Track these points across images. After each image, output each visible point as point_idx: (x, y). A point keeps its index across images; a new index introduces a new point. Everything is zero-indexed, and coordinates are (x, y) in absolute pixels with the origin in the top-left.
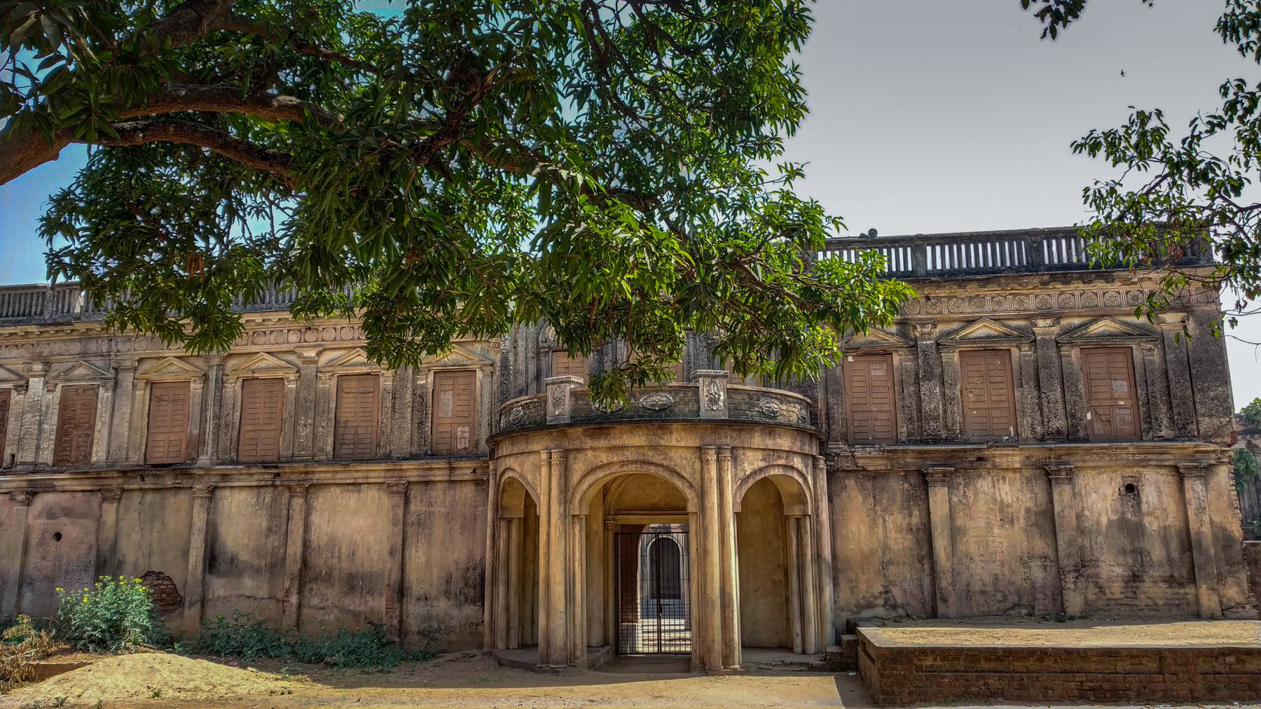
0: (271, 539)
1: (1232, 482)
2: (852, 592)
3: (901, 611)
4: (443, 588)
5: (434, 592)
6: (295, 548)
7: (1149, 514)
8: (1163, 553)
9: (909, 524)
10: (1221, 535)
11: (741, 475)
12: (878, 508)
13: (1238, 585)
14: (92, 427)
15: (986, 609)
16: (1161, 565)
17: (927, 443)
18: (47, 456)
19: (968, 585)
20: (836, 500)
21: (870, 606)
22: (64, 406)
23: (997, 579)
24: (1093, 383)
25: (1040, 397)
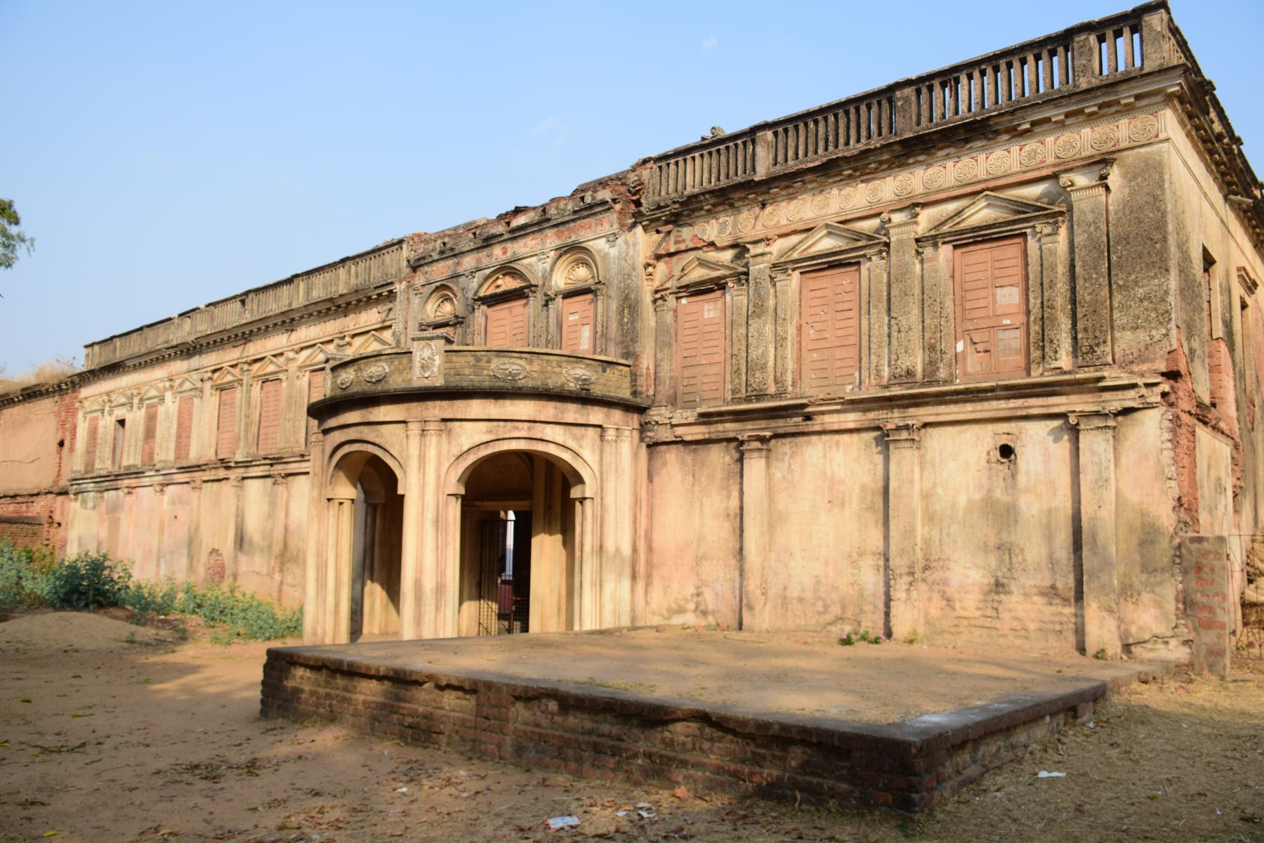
2: (665, 593)
3: (711, 619)
6: (279, 533)
7: (1027, 490)
8: (1044, 551)
9: (727, 508)
10: (1138, 523)
11: (456, 451)
12: (696, 488)
13: (1159, 605)
15: (803, 622)
20: (656, 480)
21: (681, 611)
23: (818, 582)
25: (890, 327)
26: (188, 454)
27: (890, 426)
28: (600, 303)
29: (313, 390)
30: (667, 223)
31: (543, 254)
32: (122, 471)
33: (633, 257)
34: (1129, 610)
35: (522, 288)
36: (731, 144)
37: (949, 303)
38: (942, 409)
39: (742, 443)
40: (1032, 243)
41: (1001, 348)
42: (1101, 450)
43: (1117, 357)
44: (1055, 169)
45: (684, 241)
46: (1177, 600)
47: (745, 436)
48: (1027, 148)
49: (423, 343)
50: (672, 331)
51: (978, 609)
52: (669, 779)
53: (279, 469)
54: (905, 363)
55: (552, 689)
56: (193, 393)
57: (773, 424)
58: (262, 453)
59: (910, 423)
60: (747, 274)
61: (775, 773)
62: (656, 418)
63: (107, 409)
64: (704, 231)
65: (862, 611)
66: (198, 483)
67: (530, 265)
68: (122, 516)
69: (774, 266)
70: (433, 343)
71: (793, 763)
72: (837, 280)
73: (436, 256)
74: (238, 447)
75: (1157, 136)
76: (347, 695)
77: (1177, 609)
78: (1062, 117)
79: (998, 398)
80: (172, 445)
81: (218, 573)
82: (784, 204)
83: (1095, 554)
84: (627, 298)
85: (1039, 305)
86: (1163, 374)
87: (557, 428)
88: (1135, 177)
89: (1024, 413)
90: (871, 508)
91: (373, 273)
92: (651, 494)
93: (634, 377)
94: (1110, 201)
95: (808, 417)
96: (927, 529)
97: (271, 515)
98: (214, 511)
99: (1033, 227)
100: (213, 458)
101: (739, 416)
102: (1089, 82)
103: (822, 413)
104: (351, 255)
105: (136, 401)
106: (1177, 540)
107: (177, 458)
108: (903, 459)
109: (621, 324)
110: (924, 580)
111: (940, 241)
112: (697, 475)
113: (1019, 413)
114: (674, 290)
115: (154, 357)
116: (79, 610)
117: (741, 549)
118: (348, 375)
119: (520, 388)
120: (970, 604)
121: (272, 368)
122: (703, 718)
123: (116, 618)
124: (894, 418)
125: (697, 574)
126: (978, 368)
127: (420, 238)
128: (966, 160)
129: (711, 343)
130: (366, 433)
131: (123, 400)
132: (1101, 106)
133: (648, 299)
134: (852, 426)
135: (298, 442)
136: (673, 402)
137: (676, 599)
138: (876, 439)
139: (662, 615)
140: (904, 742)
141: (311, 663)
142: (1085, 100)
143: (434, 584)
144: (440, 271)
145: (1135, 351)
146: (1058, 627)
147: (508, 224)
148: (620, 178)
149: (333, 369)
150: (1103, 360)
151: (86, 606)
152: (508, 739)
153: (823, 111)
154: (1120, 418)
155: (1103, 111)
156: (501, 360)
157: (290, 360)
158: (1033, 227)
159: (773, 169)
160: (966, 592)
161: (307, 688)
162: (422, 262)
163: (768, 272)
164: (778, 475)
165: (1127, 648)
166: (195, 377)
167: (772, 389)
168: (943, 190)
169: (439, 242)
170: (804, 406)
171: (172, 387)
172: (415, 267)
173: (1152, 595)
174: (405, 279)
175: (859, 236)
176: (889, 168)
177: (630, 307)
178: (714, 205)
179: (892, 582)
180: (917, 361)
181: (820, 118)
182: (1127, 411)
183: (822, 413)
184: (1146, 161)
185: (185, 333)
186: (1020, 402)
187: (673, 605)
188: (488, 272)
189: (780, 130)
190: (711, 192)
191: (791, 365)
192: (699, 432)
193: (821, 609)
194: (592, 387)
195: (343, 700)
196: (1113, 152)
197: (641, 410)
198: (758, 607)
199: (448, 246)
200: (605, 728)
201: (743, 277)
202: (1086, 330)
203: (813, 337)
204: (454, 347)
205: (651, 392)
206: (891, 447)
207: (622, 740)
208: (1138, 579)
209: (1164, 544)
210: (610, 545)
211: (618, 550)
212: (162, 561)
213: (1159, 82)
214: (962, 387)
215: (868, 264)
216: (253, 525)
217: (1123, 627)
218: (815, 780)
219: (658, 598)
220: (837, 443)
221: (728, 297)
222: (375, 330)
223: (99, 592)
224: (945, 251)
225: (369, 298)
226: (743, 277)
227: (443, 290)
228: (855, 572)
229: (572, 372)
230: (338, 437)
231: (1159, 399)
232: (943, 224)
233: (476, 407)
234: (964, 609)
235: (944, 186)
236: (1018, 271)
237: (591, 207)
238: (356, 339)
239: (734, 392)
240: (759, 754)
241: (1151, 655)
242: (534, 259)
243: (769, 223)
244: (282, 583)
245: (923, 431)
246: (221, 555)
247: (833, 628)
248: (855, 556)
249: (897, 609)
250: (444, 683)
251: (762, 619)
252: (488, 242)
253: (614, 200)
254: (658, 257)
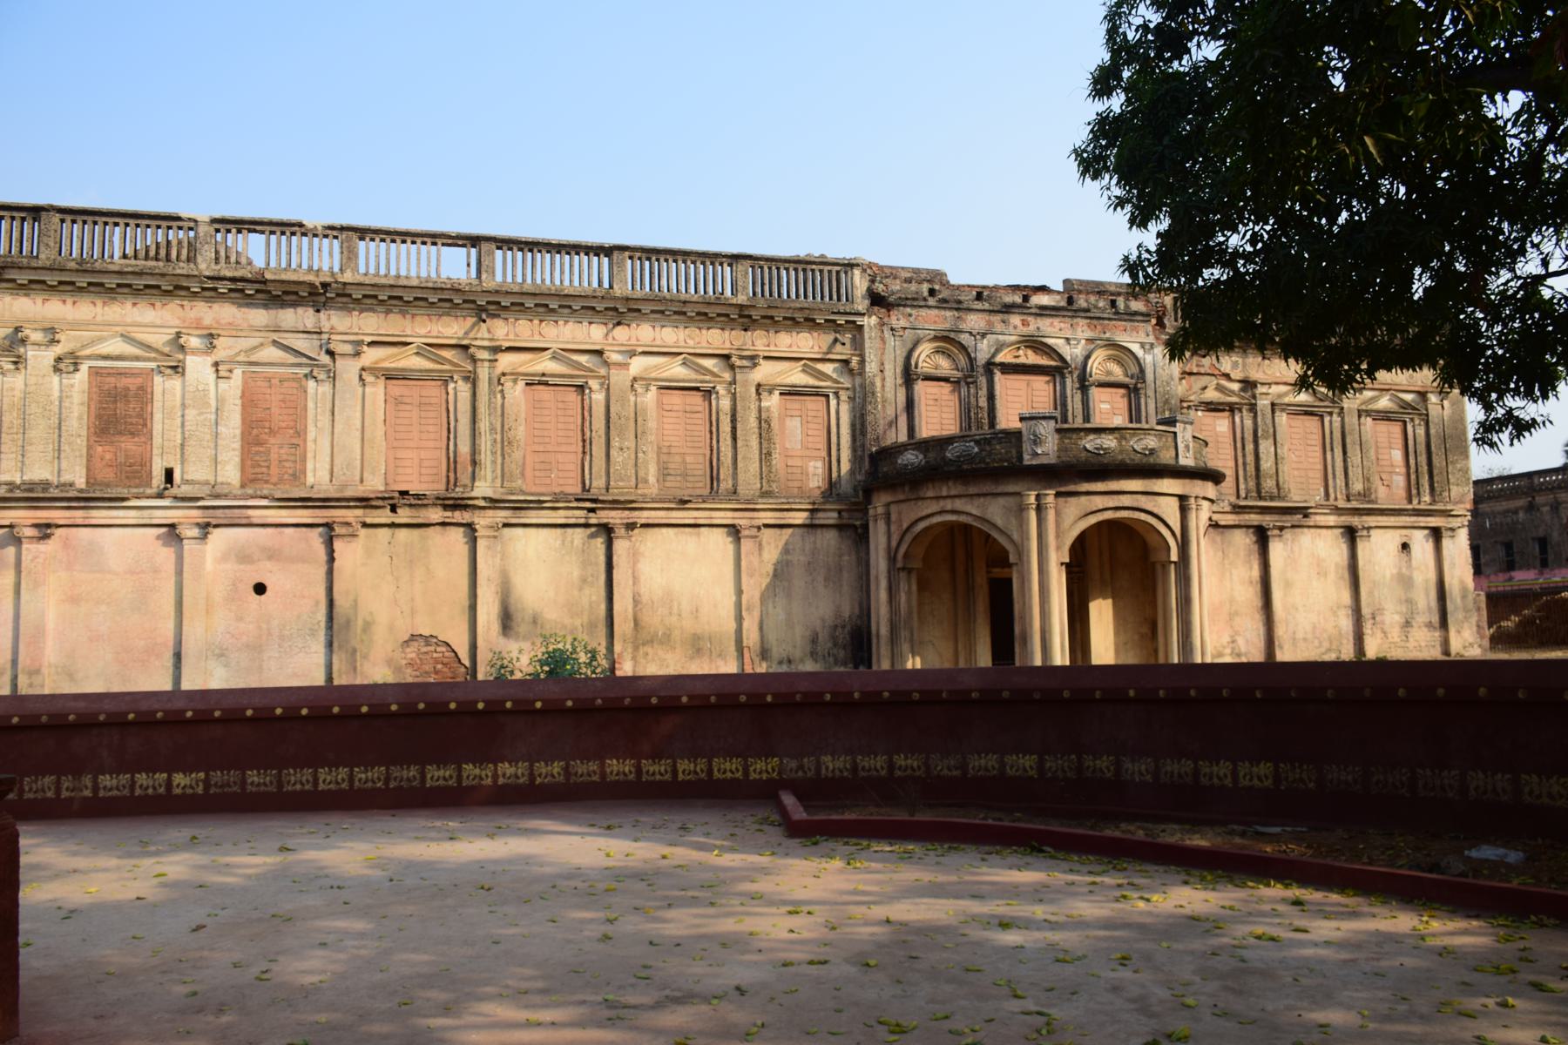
0: (587, 591)
4: (808, 649)
5: (798, 654)
14: (301, 433)
18: (230, 474)
22: (249, 401)
95: (1306, 516)
130: (1144, 502)
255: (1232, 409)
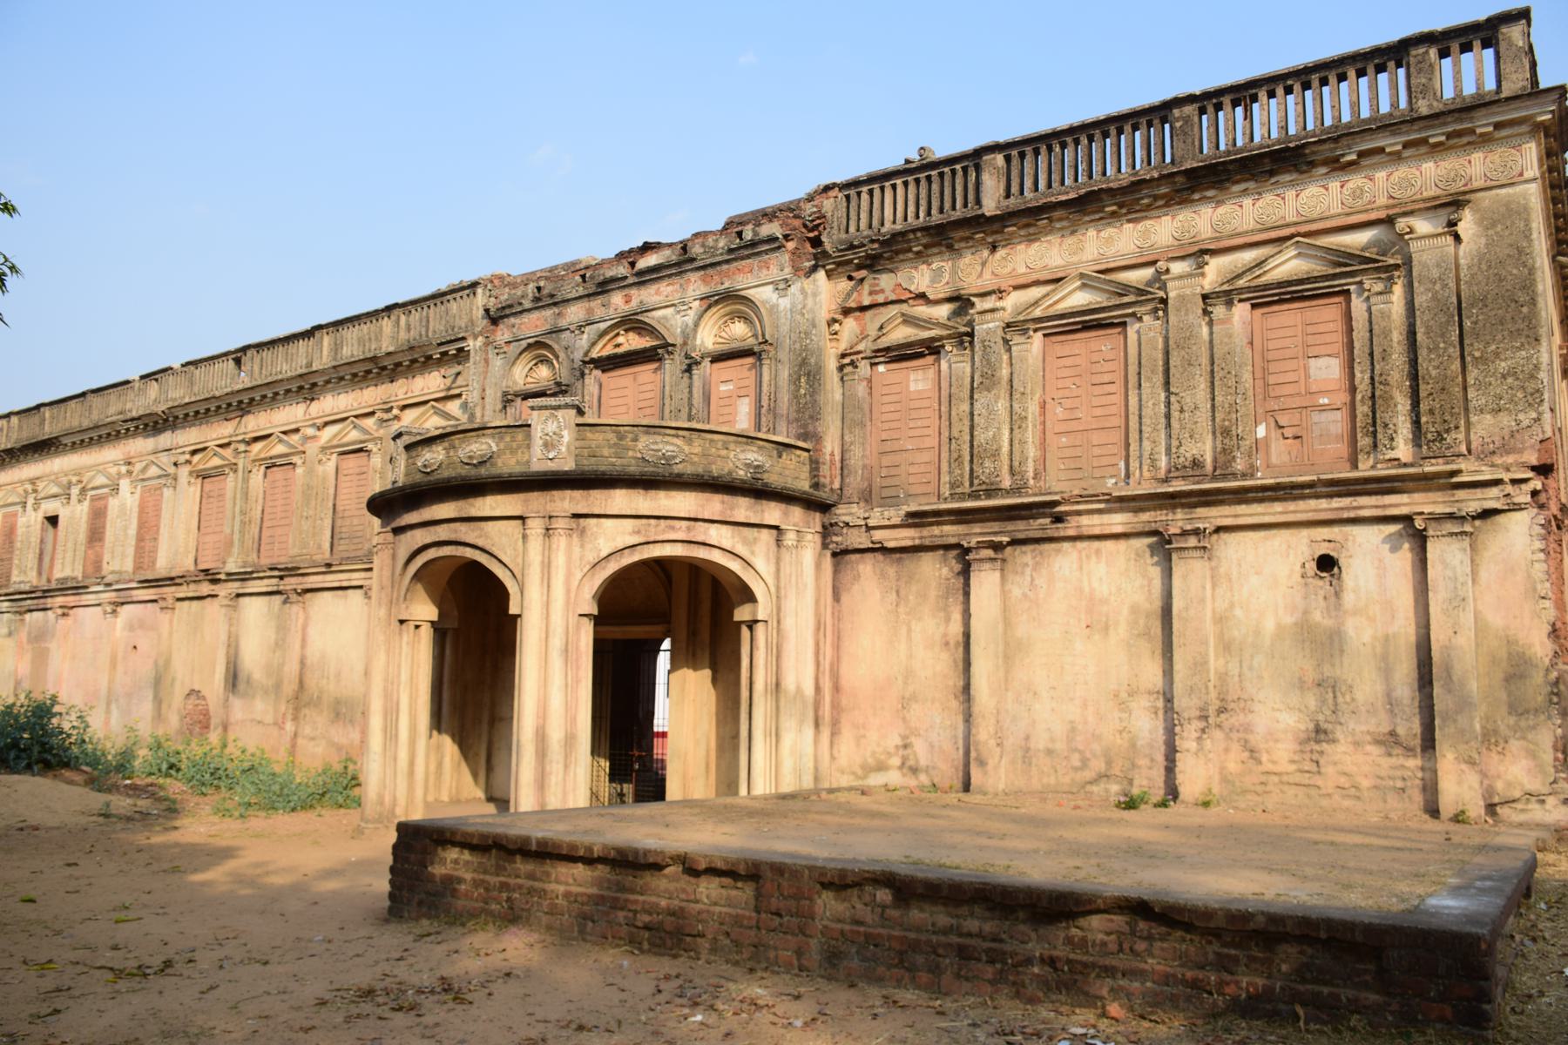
1: (1539, 545)
2: (858, 745)
6: (292, 668)
7: (1356, 612)
8: (1380, 688)
9: (945, 635)
10: (1503, 653)
11: (592, 557)
12: (901, 609)
13: (1532, 755)
15: (1052, 780)
16: (1372, 710)
17: (978, 498)
19: (1027, 738)
20: (845, 598)
21: (881, 767)
23: (1073, 730)
24: (1272, 367)
25: (1168, 404)
26: (154, 563)
27: (1172, 531)
28: (765, 370)
29: (342, 478)
30: (859, 267)
31: (684, 304)
32: (53, 585)
33: (812, 311)
34: (1493, 761)
35: (654, 348)
36: (946, 170)
37: (1247, 376)
38: (1242, 509)
39: (968, 551)
40: (1358, 304)
41: (1316, 433)
42: (1456, 562)
43: (1473, 446)
44: (1391, 212)
45: (882, 291)
46: (1556, 749)
47: (974, 541)
48: (1351, 185)
49: (547, 413)
50: (866, 407)
51: (1293, 762)
52: (1086, 994)
53: (291, 583)
54: (1190, 450)
55: (883, 873)
56: (162, 481)
57: (1010, 526)
58: (265, 561)
59: (1201, 526)
60: (971, 335)
61: (1260, 982)
62: (846, 519)
63: (31, 501)
64: (911, 279)
65: (1134, 765)
66: (170, 601)
67: (665, 318)
68: (53, 645)
69: (1008, 325)
70: (560, 413)
71: (1284, 967)
72: (1094, 345)
73: (527, 304)
74: (229, 554)
75: (1521, 174)
76: (537, 884)
77: (1556, 759)
78: (1399, 147)
79: (1317, 497)
80: (131, 551)
81: (201, 722)
82: (1021, 247)
83: (1450, 691)
84: (804, 362)
85: (1367, 380)
86: (1533, 468)
87: (724, 529)
88: (1493, 225)
89: (1352, 514)
90: (1146, 634)
91: (436, 324)
92: (838, 617)
93: (815, 465)
94: (1461, 253)
95: (1059, 519)
96: (1221, 661)
97: (280, 644)
98: (192, 640)
99: (1361, 283)
100: (192, 568)
101: (963, 516)
102: (1430, 106)
103: (1079, 513)
104: (400, 301)
105: (75, 491)
106: (1554, 674)
107: (138, 567)
108: (1190, 573)
109: (796, 396)
110: (1219, 726)
111: (1236, 298)
112: (903, 593)
113: (1346, 515)
114: (869, 354)
115: (104, 432)
116: (18, 773)
117: (967, 688)
118: (434, 456)
119: (679, 475)
120: (1282, 755)
121: (281, 449)
122: (1139, 909)
123: (71, 782)
124: (1177, 520)
125: (904, 719)
126: (1286, 458)
127: (501, 280)
128: (1269, 198)
129: (919, 423)
130: (464, 532)
131: (55, 490)
132: (1449, 136)
133: (832, 364)
134: (1119, 529)
135: (320, 547)
136: (867, 497)
137: (874, 753)
138: (1150, 546)
139: (853, 773)
140: (1469, 935)
141: (475, 841)
142: (1432, 127)
143: (562, 735)
144: (533, 324)
145: (1496, 439)
146: (1399, 784)
147: (633, 264)
148: (791, 209)
149: (408, 448)
150: (1455, 450)
151: (29, 767)
152: (813, 942)
153: (1073, 131)
154: (1477, 523)
155: (1451, 142)
156: (652, 439)
157: (307, 438)
158: (1361, 283)
159: (1005, 203)
160: (1277, 741)
161: (468, 876)
162: (508, 311)
163: (1000, 332)
164: (1016, 592)
165: (1491, 808)
166: (165, 459)
167: (1007, 483)
168: (1239, 234)
169: (532, 286)
170: (1055, 504)
171: (130, 473)
172: (495, 318)
173: (1522, 742)
174: (481, 333)
175: (1126, 289)
176: (1167, 205)
177: (808, 375)
178: (926, 246)
179: (1178, 729)
180: (1205, 448)
181: (1069, 140)
182: (1487, 514)
183: (1079, 513)
184: (1507, 205)
185: (151, 400)
186: (1346, 502)
187: (870, 760)
188: (603, 326)
189: (1014, 153)
190: (925, 229)
191: (1032, 452)
192: (907, 537)
193: (1078, 764)
194: (765, 476)
195: (531, 891)
196: (1465, 193)
197: (824, 507)
198: (991, 763)
199: (545, 292)
200: (972, 925)
201: (965, 339)
202: (1431, 412)
203: (1061, 417)
204: (588, 419)
205: (836, 485)
206: (1174, 556)
207: (1001, 941)
208: (1505, 722)
209: (1538, 678)
210: (789, 683)
211: (799, 690)
212: (113, 706)
213: (1527, 107)
214: (1272, 481)
215: (1137, 325)
216: (253, 656)
217: (1486, 782)
218: (1326, 990)
219: (848, 753)
220: (1098, 552)
221: (944, 365)
222: (436, 400)
223: (45, 747)
224: (1241, 311)
225: (429, 358)
226: (965, 339)
227: (539, 348)
228: (1124, 715)
229: (742, 456)
230: (420, 537)
231: (1528, 498)
232: (1239, 276)
233: (620, 500)
234: (1274, 762)
235: (1240, 230)
236: (1338, 338)
237: (753, 244)
238: (407, 412)
239: (953, 485)
240: (1228, 956)
241: (1522, 818)
242: (671, 310)
243: (999, 271)
244: (296, 735)
245: (1215, 537)
246: (204, 698)
247: (1095, 789)
248: (1124, 695)
249: (1184, 763)
250: (702, 866)
251: (995, 777)
252: (605, 287)
253: (786, 237)
254: (847, 312)
255: (932, 349)
